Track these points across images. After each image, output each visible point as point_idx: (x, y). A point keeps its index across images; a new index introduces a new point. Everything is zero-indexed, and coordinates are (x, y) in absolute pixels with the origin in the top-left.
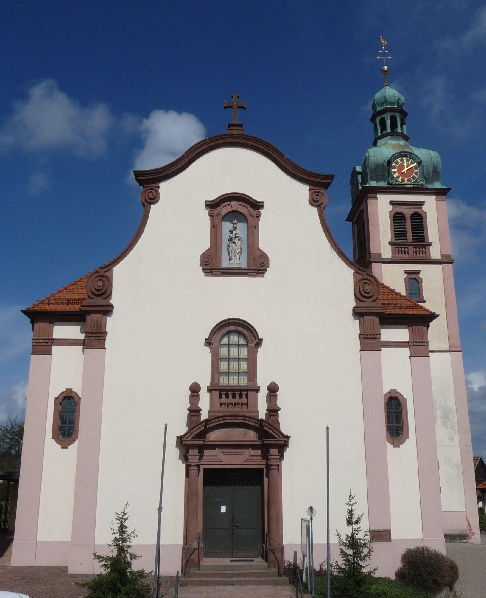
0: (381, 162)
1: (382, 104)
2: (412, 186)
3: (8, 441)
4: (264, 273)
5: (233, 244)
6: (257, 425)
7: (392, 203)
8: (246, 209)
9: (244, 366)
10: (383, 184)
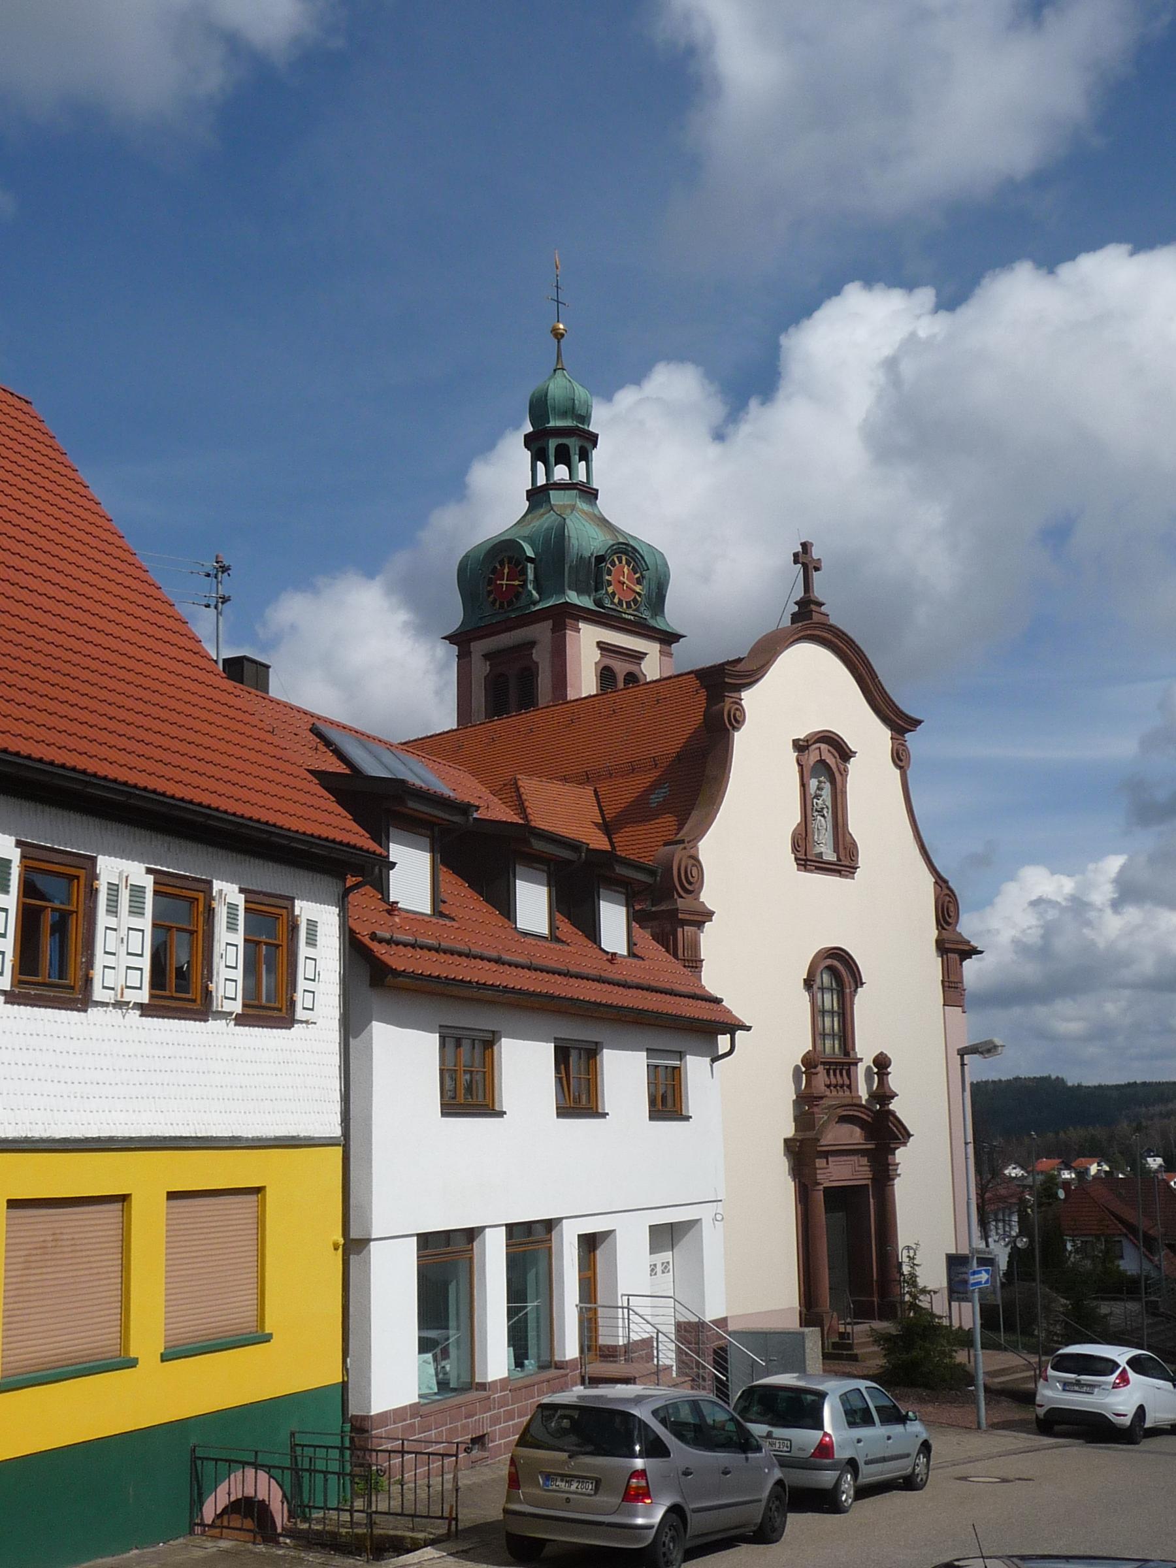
0: (587, 554)
1: (564, 414)
7: (602, 646)
10: (586, 602)
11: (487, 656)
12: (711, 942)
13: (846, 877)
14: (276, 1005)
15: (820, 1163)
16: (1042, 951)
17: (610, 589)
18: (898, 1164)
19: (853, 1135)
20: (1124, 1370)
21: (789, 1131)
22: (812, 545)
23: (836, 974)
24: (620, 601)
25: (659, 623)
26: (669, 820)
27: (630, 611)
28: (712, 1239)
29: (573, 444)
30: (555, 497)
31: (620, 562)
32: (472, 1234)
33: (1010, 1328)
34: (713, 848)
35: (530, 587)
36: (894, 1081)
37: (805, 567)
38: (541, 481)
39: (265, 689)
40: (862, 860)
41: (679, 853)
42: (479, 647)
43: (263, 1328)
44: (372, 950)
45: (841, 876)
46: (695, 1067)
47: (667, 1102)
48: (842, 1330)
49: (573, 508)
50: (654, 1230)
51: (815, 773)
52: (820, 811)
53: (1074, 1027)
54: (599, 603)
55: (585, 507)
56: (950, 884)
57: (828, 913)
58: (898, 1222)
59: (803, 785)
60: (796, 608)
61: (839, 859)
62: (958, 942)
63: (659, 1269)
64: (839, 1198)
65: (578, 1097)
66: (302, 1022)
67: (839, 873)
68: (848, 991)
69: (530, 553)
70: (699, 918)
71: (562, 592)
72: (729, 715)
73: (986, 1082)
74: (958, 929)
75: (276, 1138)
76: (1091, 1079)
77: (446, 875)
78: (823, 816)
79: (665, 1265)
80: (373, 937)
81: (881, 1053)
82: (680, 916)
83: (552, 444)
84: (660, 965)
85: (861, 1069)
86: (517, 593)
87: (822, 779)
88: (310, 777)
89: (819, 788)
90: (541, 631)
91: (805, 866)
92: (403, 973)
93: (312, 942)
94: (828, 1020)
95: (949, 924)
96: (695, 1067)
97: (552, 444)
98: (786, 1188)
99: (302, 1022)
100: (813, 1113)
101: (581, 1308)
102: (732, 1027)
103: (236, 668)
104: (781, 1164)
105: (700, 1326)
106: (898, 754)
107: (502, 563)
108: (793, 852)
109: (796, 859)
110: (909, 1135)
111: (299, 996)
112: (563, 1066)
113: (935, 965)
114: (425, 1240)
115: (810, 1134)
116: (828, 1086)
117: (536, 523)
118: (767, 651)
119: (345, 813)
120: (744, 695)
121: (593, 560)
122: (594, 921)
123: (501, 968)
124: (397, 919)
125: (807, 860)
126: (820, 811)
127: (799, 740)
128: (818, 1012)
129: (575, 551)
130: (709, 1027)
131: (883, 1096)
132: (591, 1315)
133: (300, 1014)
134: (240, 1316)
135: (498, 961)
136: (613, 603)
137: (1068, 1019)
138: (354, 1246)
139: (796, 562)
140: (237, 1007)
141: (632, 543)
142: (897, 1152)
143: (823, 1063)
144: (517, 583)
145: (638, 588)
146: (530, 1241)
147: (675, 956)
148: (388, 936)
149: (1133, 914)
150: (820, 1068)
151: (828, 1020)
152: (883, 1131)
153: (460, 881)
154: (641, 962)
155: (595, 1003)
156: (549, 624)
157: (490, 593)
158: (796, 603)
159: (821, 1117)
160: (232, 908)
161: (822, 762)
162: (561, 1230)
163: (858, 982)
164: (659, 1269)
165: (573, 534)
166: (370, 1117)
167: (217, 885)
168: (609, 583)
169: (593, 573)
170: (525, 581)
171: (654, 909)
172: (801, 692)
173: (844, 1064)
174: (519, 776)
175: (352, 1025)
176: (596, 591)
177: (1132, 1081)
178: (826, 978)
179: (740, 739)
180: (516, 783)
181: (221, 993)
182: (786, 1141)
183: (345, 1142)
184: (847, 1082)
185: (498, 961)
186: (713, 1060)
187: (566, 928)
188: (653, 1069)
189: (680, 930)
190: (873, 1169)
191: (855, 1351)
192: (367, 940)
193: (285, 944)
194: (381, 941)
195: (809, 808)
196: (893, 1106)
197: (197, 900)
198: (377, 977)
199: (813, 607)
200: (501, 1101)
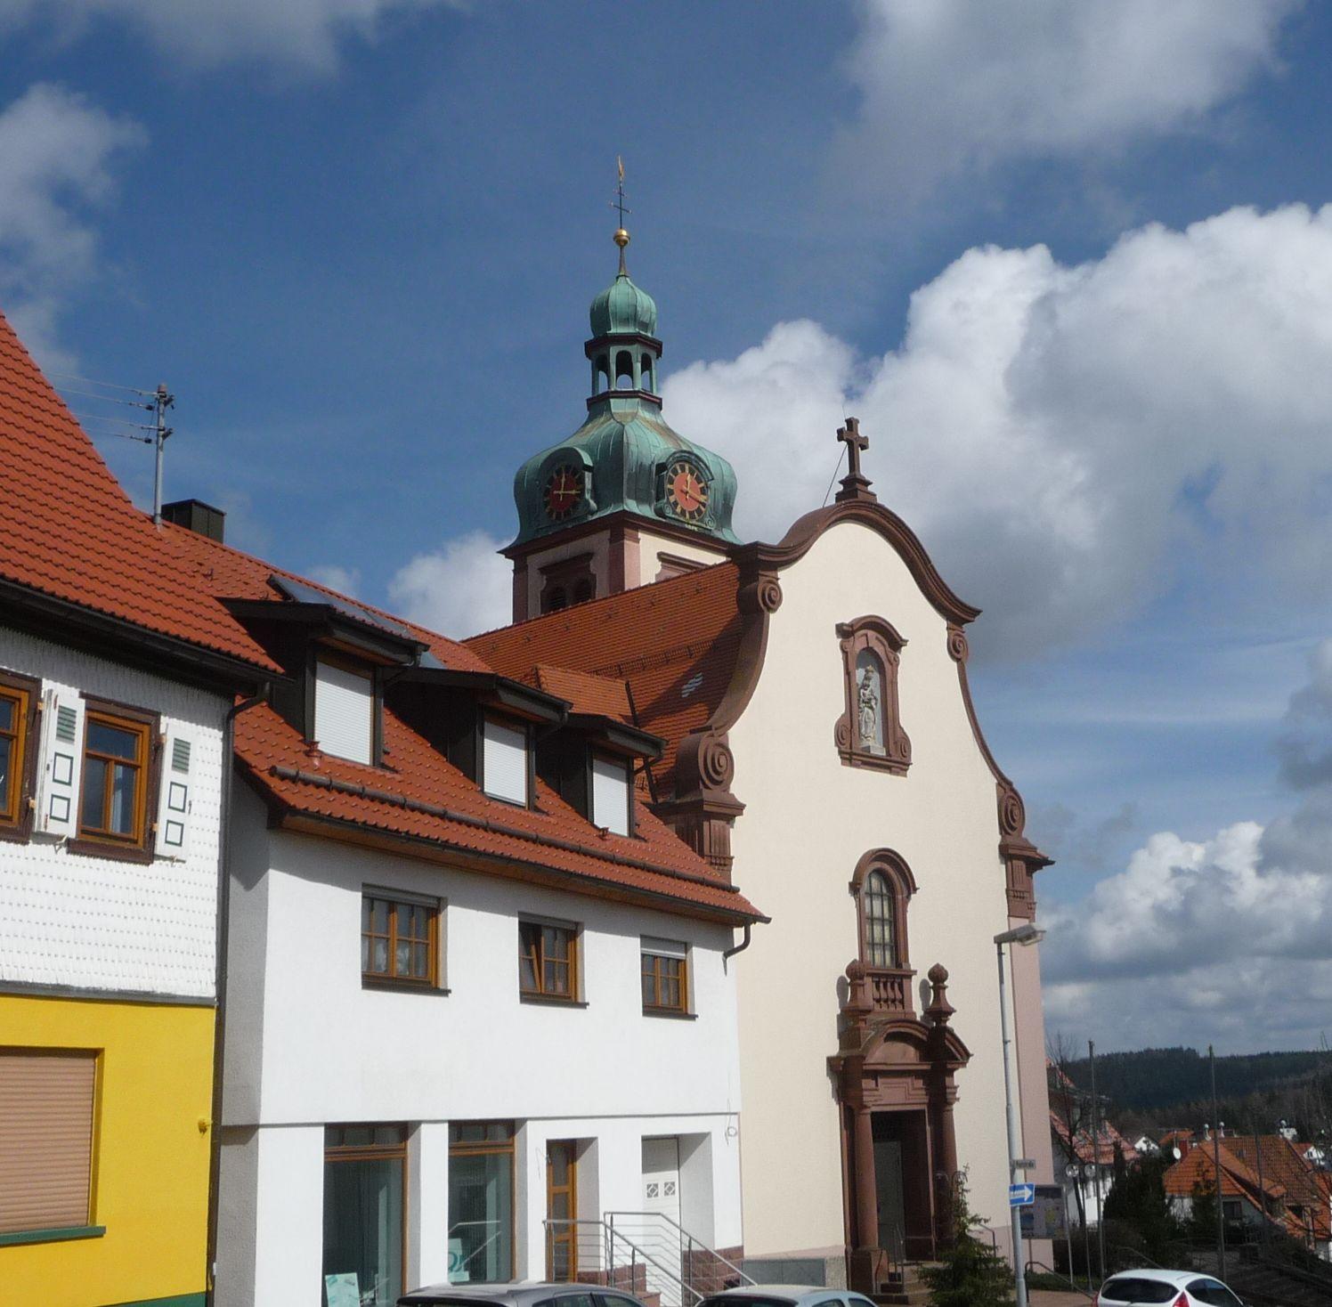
0: (647, 462)
1: (626, 321)
2: (696, 529)
3: (1157, 1110)
4: (906, 770)
5: (870, 711)
6: (924, 1038)
7: (664, 558)
8: (882, 648)
9: (607, 896)
10: (647, 511)
11: (543, 570)
12: (742, 838)
13: (897, 774)
14: (131, 836)
15: (867, 1083)
16: (1178, 918)
17: (672, 499)
18: (956, 1088)
19: (907, 1055)
20: (1183, 1297)
21: (834, 1048)
22: (857, 421)
23: (885, 879)
24: (683, 512)
25: (726, 535)
26: (700, 709)
27: (694, 522)
28: (723, 1155)
29: (636, 351)
30: (615, 404)
31: (683, 470)
32: (405, 1130)
33: (1080, 1270)
34: (744, 737)
35: (588, 496)
36: (951, 996)
37: (850, 444)
38: (602, 388)
39: (219, 538)
40: (915, 755)
41: (705, 742)
42: (535, 561)
43: (94, 1221)
44: (268, 786)
45: (891, 772)
46: (704, 962)
47: (667, 995)
48: (892, 1270)
49: (634, 416)
50: (649, 1142)
51: (861, 662)
52: (868, 702)
53: (1212, 997)
54: (660, 512)
55: (647, 415)
56: (1014, 786)
57: (876, 811)
58: (957, 1145)
59: (848, 673)
60: (841, 488)
61: (888, 754)
62: (1023, 848)
63: (661, 1189)
64: (892, 1126)
65: (549, 976)
66: (165, 858)
67: (888, 769)
68: (900, 897)
69: (587, 461)
70: (727, 811)
71: (621, 500)
72: (763, 595)
73: (1117, 1055)
74: (1025, 834)
75: (121, 992)
76: (1224, 1050)
77: (387, 718)
78: (871, 708)
79: (669, 1188)
80: (273, 771)
81: (938, 966)
82: (706, 808)
83: (614, 351)
84: (666, 845)
85: (915, 983)
86: (577, 501)
87: (870, 668)
88: (218, 605)
89: (867, 678)
90: (599, 543)
91: (850, 760)
92: (305, 813)
93: (181, 763)
94: (877, 929)
95: (1013, 828)
96: (704, 962)
97: (614, 351)
98: (829, 1114)
99: (165, 858)
100: (859, 1029)
101: (549, 1225)
102: (748, 918)
103: (180, 513)
104: (823, 1087)
105: (707, 1256)
106: (954, 645)
107: (559, 473)
108: (836, 745)
109: (840, 752)
110: (968, 1055)
111: (160, 828)
112: (533, 948)
113: (997, 874)
114: (337, 1133)
115: (855, 1052)
116: (878, 1001)
117: (595, 432)
118: (805, 532)
119: (256, 646)
120: (781, 574)
121: (654, 469)
122: (586, 798)
123: (447, 824)
124: (316, 762)
125: (852, 752)
126: (868, 702)
127: (842, 624)
128: (865, 920)
129: (634, 458)
130: (725, 920)
131: (939, 1012)
132: (567, 1235)
133: (161, 848)
134: (61, 1204)
135: (443, 816)
136: (674, 512)
137: (1203, 988)
138: (231, 1134)
139: (840, 438)
140: (70, 830)
141: (696, 451)
142: (955, 1073)
143: (872, 975)
144: (574, 492)
145: (702, 498)
146: (482, 1148)
147: (701, 854)
148: (292, 772)
149: (1271, 883)
150: (868, 980)
151: (877, 929)
152: (939, 1051)
153: (420, 740)
154: (643, 843)
155: (566, 872)
156: (606, 534)
157: (546, 503)
158: (841, 482)
159: (868, 1033)
160: (66, 716)
161: (869, 650)
162: (525, 1130)
163: (911, 887)
164: (661, 1189)
165: (633, 441)
166: (262, 981)
167: (47, 685)
168: (671, 492)
169: (657, 479)
170: (583, 490)
171: (678, 801)
172: (844, 578)
173: (896, 976)
174: (540, 665)
175: (238, 866)
176: (658, 500)
177: (1265, 1051)
178: (875, 883)
179: (775, 621)
180: (537, 673)
181: (45, 810)
182: (830, 1060)
183: (219, 1004)
184: (899, 996)
185: (443, 816)
186: (727, 955)
187: (549, 799)
188: (648, 962)
189: (706, 824)
190: (929, 1093)
191: (906, 1293)
192: (265, 776)
193: (145, 765)
194: (284, 777)
195: (855, 697)
196: (951, 1023)
197: (19, 700)
198: (272, 817)
199: (859, 486)
200: (445, 977)
